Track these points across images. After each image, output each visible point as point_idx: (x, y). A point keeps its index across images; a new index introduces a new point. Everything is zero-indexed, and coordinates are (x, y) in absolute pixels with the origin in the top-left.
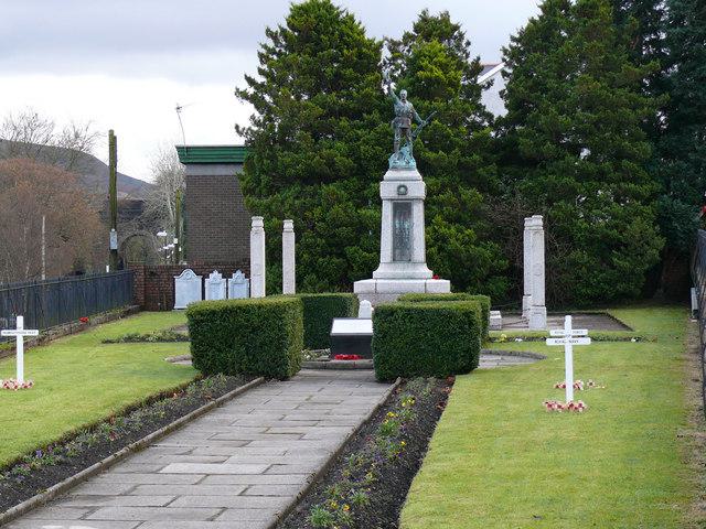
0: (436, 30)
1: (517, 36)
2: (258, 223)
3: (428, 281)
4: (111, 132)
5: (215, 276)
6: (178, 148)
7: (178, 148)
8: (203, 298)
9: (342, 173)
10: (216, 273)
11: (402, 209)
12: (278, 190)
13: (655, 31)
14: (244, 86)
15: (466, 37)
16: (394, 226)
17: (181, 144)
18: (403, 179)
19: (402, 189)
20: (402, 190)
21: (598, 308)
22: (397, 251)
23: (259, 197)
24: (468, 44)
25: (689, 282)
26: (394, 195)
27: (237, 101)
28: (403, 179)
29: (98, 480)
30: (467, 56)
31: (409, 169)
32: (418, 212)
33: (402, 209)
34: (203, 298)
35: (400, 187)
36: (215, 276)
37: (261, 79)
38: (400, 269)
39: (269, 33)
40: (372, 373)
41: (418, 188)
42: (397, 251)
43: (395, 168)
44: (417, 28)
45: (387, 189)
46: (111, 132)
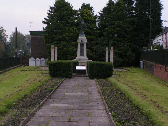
0: (86, 7)
1: (102, 10)
4: (16, 27)
5: (38, 59)
6: (30, 31)
7: (30, 31)
8: (54, 60)
10: (38, 58)
11: (82, 45)
13: (132, 11)
14: (44, 20)
15: (93, 10)
17: (30, 30)
18: (83, 38)
19: (82, 41)
20: (82, 41)
22: (81, 54)
23: (49, 44)
24: (94, 11)
25: (29, 64)
26: (80, 42)
27: (43, 24)
28: (83, 38)
30: (93, 14)
31: (84, 36)
32: (85, 46)
33: (82, 45)
34: (54, 60)
36: (38, 59)
37: (48, 19)
38: (81, 57)
39: (51, 8)
41: (85, 41)
43: (81, 36)
44: (82, 7)
45: (79, 41)
46: (16, 27)
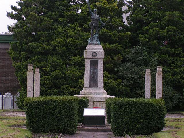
2: (148, 71)
3: (106, 96)
8: (34, 95)
9: (165, 26)
11: (94, 63)
12: (29, 58)
16: (90, 71)
18: (95, 49)
20: (94, 54)
21: (175, 111)
22: (92, 82)
26: (90, 56)
28: (95, 49)
29: (18, 124)
33: (94, 63)
35: (93, 53)
38: (93, 90)
40: (112, 133)
41: (101, 54)
42: (92, 82)
43: (91, 44)
45: (88, 54)
